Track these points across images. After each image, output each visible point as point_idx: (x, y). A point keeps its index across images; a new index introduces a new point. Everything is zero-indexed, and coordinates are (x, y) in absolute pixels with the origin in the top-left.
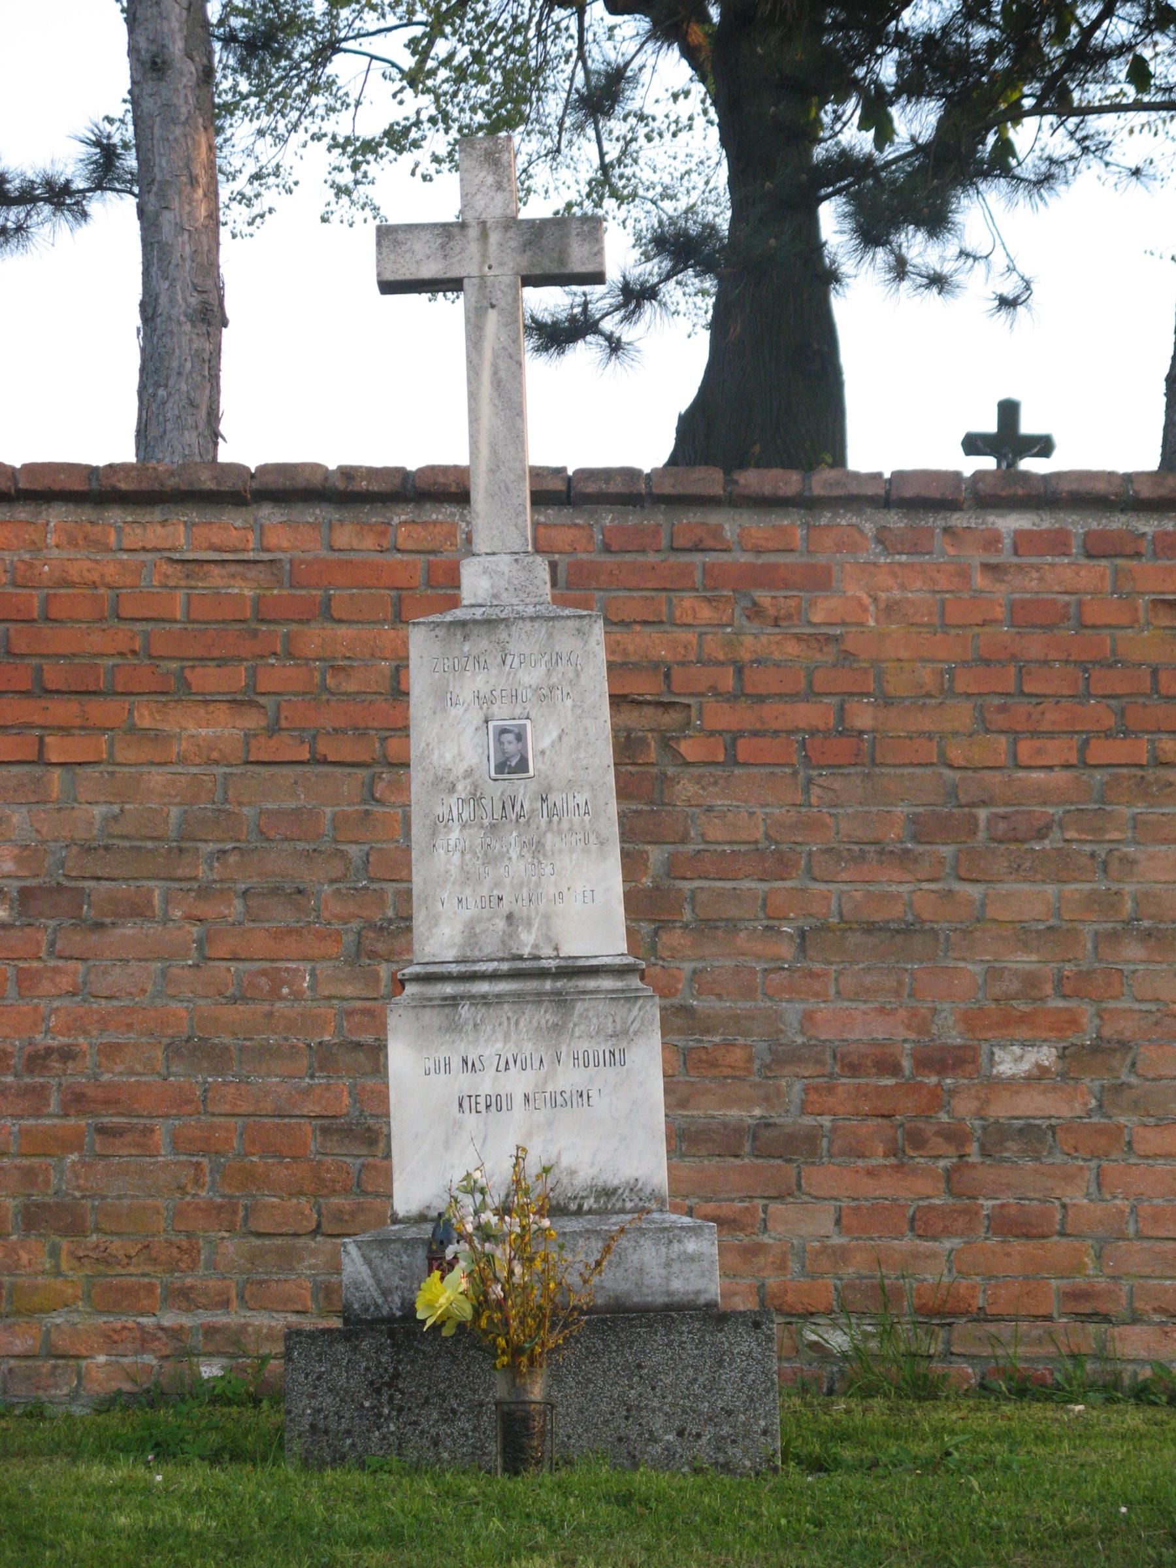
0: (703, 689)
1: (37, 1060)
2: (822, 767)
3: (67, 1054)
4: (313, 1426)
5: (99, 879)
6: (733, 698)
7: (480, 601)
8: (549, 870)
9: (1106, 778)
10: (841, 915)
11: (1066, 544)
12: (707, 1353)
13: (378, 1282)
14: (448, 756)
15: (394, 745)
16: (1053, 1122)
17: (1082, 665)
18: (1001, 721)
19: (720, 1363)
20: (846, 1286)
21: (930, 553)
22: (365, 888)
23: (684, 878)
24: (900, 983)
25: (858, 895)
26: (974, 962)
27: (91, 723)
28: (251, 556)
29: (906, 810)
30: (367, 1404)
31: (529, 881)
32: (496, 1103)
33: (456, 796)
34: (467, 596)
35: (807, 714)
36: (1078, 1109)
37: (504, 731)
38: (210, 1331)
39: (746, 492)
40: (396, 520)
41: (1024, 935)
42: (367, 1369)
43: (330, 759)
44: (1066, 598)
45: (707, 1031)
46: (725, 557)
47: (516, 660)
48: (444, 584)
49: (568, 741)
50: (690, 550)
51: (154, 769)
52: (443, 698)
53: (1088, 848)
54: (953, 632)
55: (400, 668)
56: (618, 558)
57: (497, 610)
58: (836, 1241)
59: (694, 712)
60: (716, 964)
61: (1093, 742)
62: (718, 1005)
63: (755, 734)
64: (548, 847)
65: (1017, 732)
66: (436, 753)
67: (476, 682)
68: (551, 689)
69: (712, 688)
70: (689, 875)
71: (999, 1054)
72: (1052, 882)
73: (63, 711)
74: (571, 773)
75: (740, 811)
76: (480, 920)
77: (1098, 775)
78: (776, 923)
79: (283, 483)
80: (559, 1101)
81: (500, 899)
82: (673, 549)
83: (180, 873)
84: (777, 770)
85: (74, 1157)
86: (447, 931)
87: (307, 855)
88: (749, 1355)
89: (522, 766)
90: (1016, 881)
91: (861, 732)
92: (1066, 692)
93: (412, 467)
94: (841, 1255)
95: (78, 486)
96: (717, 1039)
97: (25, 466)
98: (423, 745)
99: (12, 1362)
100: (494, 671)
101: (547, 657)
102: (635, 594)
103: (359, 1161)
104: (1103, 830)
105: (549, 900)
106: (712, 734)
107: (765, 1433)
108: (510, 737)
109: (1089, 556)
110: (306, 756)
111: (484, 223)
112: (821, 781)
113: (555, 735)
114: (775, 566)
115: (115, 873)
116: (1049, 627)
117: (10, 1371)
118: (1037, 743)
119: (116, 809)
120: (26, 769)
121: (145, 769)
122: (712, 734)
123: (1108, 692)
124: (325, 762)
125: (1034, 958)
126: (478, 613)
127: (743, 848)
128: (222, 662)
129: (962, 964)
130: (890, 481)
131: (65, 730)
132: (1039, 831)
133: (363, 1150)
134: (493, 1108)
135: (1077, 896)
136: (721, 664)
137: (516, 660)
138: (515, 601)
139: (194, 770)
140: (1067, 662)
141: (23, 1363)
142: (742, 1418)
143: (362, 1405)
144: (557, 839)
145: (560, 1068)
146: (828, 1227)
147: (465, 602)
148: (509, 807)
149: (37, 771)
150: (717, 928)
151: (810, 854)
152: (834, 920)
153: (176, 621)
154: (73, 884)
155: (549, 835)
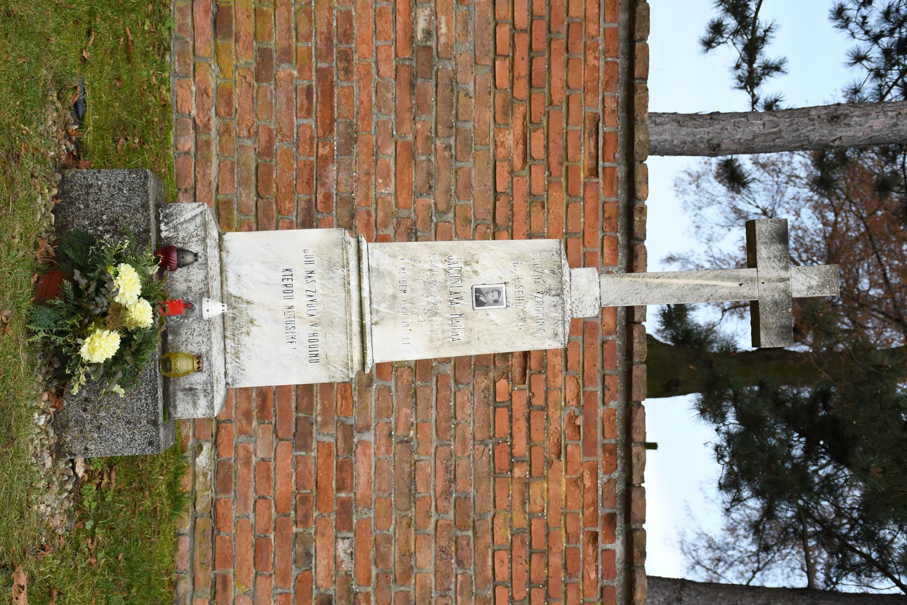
1: (346, 56)
2: (493, 452)
3: (347, 71)
4: (91, 186)
5: (437, 86)
6: (529, 403)
7: (573, 279)
8: (421, 319)
9: (489, 597)
10: (419, 460)
11: (608, 577)
12: (134, 414)
13: (181, 224)
15: (505, 234)
16: (313, 570)
17: (546, 583)
18: (517, 543)
19: (129, 422)
20: (230, 466)
21: (603, 506)
22: (432, 221)
23: (437, 381)
24: (384, 491)
25: (428, 470)
26: (395, 529)
27: (515, 81)
28: (601, 162)
29: (472, 494)
30: (104, 217)
32: (288, 290)
33: (463, 266)
34: (576, 271)
35: (521, 447)
36: (320, 582)
37: (499, 293)
38: (208, 143)
39: (634, 413)
40: (619, 235)
41: (407, 555)
42: (125, 218)
43: (498, 203)
44: (581, 576)
45: (360, 395)
46: (600, 403)
48: (581, 260)
50: (603, 384)
51: (492, 114)
52: (518, 259)
53: (453, 587)
54: (563, 518)
55: (541, 236)
56: (599, 347)
57: (568, 289)
58: (254, 459)
61: (507, 590)
62: (373, 399)
63: (511, 417)
64: (434, 318)
65: (511, 551)
67: (526, 276)
68: (523, 320)
70: (439, 384)
71: (347, 542)
72: (435, 569)
73: (522, 68)
75: (469, 410)
76: (393, 280)
77: (490, 592)
78: (415, 428)
79: (639, 178)
80: (290, 325)
82: (604, 376)
83: (440, 127)
84: (492, 428)
85: (295, 73)
86: (386, 261)
87: (449, 191)
88: (132, 440)
89: (479, 303)
90: (436, 551)
91: (511, 471)
92: (532, 576)
93: (646, 243)
94: (247, 463)
95: (637, 72)
96: (355, 399)
97: (647, 45)
99: (192, 43)
100: (534, 287)
101: (541, 317)
103: (294, 219)
104: (462, 596)
106: (511, 395)
107: (86, 449)
108: (496, 294)
109: (602, 589)
110: (498, 190)
111: (788, 279)
112: (487, 450)
113: (497, 321)
114: (596, 428)
115: (439, 94)
116: (565, 567)
117: (187, 42)
118: (506, 561)
119: (472, 94)
120: (492, 47)
121: (492, 109)
122: (511, 395)
123: (532, 598)
124: (496, 199)
125: (397, 559)
126: (566, 278)
127: (452, 411)
128: (547, 147)
129: (393, 522)
130: (640, 486)
131: (512, 69)
132: (462, 562)
133: (299, 221)
134: (285, 288)
135: (428, 581)
136: (546, 399)
137: (540, 300)
138: (573, 299)
139: (492, 134)
140: (548, 576)
141: (191, 48)
142: (96, 435)
143: (103, 214)
144: (439, 323)
145: (308, 326)
146: (260, 455)
149: (492, 55)
151: (450, 445)
152: (416, 457)
153: (567, 124)
154: (434, 73)
155: (441, 319)
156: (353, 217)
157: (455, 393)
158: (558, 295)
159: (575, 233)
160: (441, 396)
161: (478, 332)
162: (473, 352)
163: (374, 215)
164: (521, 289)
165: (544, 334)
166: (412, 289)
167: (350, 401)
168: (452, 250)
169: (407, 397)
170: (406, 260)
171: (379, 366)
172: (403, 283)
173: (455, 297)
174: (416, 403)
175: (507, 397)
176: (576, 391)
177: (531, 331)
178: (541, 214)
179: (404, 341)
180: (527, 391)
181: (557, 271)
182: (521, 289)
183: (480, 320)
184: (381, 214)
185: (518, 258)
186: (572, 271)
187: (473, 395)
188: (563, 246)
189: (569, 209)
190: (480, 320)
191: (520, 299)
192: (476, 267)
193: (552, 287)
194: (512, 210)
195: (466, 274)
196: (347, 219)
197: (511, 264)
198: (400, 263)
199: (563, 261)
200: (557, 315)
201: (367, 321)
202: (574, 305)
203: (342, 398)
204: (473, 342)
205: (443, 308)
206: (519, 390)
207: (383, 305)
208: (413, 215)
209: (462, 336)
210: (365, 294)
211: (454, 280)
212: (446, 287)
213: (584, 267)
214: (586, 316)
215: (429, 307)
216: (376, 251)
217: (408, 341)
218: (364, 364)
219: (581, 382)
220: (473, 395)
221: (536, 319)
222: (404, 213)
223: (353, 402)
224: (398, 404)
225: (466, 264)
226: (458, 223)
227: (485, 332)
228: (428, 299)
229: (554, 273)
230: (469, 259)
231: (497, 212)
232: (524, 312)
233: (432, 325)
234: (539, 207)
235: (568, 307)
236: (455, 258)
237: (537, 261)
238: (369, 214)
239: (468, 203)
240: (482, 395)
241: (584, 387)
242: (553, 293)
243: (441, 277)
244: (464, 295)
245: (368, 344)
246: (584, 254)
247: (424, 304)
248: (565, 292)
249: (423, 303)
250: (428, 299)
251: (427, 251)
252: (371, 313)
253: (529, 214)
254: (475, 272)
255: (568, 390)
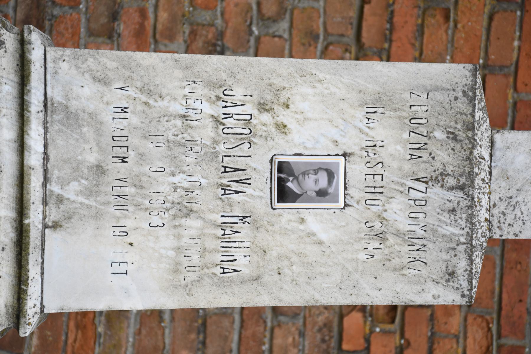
0: (407, 335)
7: (497, 154)
8: (156, 221)
14: (304, 106)
22: (251, 33)
31: (145, 197)
33: (255, 112)
34: (506, 138)
37: (331, 175)
47: (419, 195)
49: (312, 251)
52: (375, 105)
57: (484, 175)
59: (389, 327)
60: (167, 331)
62: (131, 331)
64: (186, 222)
66: (310, 91)
67: (393, 141)
68: (381, 237)
69: (408, 343)
74: (274, 253)
76: (99, 133)
81: (124, 160)
86: (86, 91)
89: (284, 195)
96: (100, 329)
98: (321, 75)
100: (407, 167)
101: (420, 232)
102: (497, 283)
105: (118, 218)
106: (368, 340)
108: (323, 182)
113: (323, 236)
122: (368, 340)
137: (419, 195)
138: (495, 197)
144: (194, 232)
147: (498, 137)
148: (237, 176)
150: (199, 333)
156: (114, 16)
157: (272, 330)
158: (462, 188)
159: (502, 67)
160: (247, 333)
161: (279, 257)
162: (265, 300)
163: (151, 15)
164: (379, 169)
165: (425, 272)
166: (141, 156)
167: (90, 333)
168: (232, 75)
169: (189, 332)
170: (131, 92)
171: (50, 321)
172: (120, 141)
173: (233, 179)
174: (204, 343)
175: (361, 344)
176: (485, 343)
177: (396, 261)
178: (442, 32)
179: (116, 268)
180: (398, 336)
181: (461, 135)
182: (379, 169)
183: (285, 232)
184: (163, 16)
185: (378, 101)
186: (498, 137)
187: (302, 334)
188: (479, 80)
189: (494, 24)
190: (285, 232)
191: (374, 191)
192: (285, 116)
193: (449, 169)
194: (390, 21)
195: (260, 130)
196: (104, 20)
197: (361, 113)
198: (118, 98)
199: (478, 114)
200: (455, 230)
201: (35, 217)
202: (495, 211)
203: (78, 327)
204: (266, 279)
205: (207, 200)
206: (384, 332)
207: (74, 186)
208: (219, 22)
209: (243, 263)
210: (34, 160)
211: (233, 141)
212: (216, 155)
213: (513, 128)
214: (522, 237)
215: (175, 197)
216: (64, 66)
217: (123, 268)
218: (18, 313)
219: (494, 328)
220: (302, 334)
221: (409, 238)
222: (205, 16)
223: (97, 336)
224: (173, 343)
225: (263, 107)
226: (296, 39)
227: (295, 259)
228: (175, 179)
229: (455, 138)
230: (269, 97)
231: (364, 24)
232: (382, 220)
233: (179, 237)
234: (440, 18)
235: (483, 214)
236: (238, 93)
237: (420, 111)
238: (143, 12)
239: (315, 5)
240: (319, 336)
241: (499, 336)
242: (451, 181)
243: (206, 133)
244: (253, 175)
245: (33, 271)
246: (515, 104)
247: (165, 188)
248: (478, 181)
249: (163, 186)
250: (175, 179)
251: (178, 74)
252: (45, 203)
253: (421, 30)
254: (282, 128)
255: (470, 341)
